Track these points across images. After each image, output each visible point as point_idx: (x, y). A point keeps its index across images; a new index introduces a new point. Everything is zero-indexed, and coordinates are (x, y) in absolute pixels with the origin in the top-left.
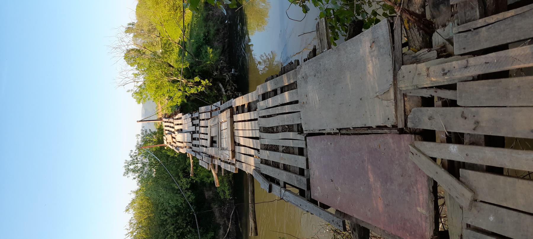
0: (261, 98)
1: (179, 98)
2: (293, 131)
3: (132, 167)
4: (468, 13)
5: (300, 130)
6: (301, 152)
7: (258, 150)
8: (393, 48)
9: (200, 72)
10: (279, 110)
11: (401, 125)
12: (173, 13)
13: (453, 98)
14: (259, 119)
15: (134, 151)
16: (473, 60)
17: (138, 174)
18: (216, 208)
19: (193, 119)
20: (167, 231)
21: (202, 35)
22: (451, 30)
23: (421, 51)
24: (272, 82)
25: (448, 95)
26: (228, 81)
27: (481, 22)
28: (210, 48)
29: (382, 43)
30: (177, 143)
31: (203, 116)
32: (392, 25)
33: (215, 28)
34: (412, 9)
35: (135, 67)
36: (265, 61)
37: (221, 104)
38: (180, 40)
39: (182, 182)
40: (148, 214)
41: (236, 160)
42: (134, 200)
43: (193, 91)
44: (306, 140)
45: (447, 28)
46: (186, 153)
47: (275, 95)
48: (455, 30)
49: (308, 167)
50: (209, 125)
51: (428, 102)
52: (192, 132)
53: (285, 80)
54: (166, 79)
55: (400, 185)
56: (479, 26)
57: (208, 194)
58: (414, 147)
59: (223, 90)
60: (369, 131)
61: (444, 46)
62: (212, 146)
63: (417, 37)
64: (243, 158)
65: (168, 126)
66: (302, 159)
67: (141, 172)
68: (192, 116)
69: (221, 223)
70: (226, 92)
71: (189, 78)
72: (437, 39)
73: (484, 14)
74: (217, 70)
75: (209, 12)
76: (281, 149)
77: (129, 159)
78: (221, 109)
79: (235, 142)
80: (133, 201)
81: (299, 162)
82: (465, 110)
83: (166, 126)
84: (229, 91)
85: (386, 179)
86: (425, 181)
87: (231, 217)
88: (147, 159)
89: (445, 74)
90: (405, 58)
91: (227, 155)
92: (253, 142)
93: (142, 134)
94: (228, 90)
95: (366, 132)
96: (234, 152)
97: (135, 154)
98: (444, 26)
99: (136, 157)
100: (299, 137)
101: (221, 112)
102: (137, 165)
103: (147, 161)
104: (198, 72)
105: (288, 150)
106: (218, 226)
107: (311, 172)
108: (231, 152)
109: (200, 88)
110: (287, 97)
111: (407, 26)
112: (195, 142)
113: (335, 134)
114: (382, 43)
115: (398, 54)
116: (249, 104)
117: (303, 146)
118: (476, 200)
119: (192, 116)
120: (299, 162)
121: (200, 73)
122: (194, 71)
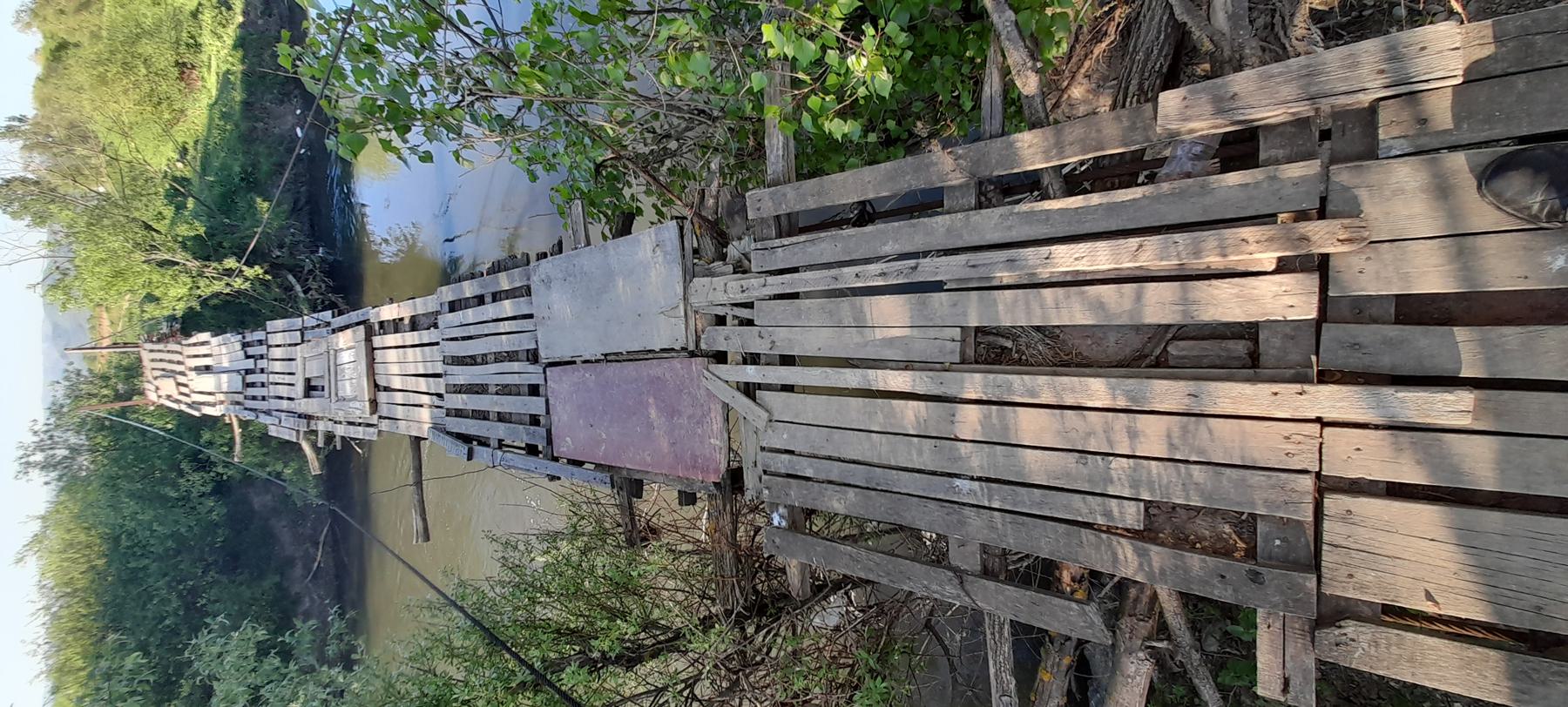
0: (446, 308)
1: (179, 300)
2: (518, 361)
3: (39, 457)
4: (765, 231)
5: (533, 356)
6: (534, 390)
7: (440, 396)
8: (683, 256)
9: (236, 248)
10: (491, 328)
11: (692, 347)
12: (149, 109)
13: (751, 317)
14: (441, 342)
15: (42, 421)
16: (771, 279)
17: (57, 473)
18: (284, 527)
19: (245, 345)
20: (150, 589)
21: (237, 169)
22: (746, 244)
23: (715, 264)
24: (475, 284)
25: (745, 313)
26: (311, 272)
27: (777, 242)
28: (264, 201)
29: (669, 249)
30: (193, 395)
31: (277, 339)
32: (681, 228)
33: (274, 159)
34: (703, 214)
35: (26, 222)
36: (397, 239)
37: (333, 317)
38: (166, 172)
39: (188, 480)
40: (89, 561)
41: (380, 417)
42: (36, 535)
43: (218, 287)
44: (545, 372)
45: (742, 242)
46: (223, 415)
47: (479, 305)
48: (753, 246)
49: (548, 412)
50: (299, 355)
51: (721, 321)
52: (243, 372)
53: (504, 282)
54: (139, 256)
55: (689, 417)
56: (775, 245)
57: (259, 501)
58: (708, 370)
59: (298, 288)
60: (650, 356)
61: (740, 261)
62: (307, 395)
63: (709, 247)
64: (400, 412)
65: (161, 360)
66: (540, 401)
67: (66, 467)
68: (244, 338)
69: (297, 555)
70: (305, 292)
71: (207, 259)
72: (733, 251)
73: (780, 235)
74: (281, 247)
75: (256, 125)
76: (493, 389)
77: (30, 439)
78: (334, 326)
79: (376, 386)
80: (37, 539)
81: (535, 405)
82: (763, 330)
83: (153, 360)
84: (313, 292)
85: (671, 412)
86: (719, 407)
87: (322, 539)
88: (83, 437)
89: (743, 291)
90: (696, 268)
91: (361, 410)
92: (427, 382)
93: (67, 379)
94: (310, 289)
95: (646, 357)
96: (374, 403)
97: (45, 428)
98: (740, 239)
99: (49, 434)
100: (531, 368)
101: (334, 331)
102: (51, 452)
103: (81, 442)
104: (230, 248)
105: (506, 390)
106: (290, 562)
107: (554, 418)
108: (367, 404)
109: (238, 283)
110: (507, 307)
111: (698, 232)
112: (251, 391)
113: (597, 361)
114: (669, 249)
115: (689, 265)
116: (413, 318)
117: (541, 382)
118: (771, 421)
119: (244, 338)
120: (535, 405)
121: (236, 251)
122: (220, 244)
